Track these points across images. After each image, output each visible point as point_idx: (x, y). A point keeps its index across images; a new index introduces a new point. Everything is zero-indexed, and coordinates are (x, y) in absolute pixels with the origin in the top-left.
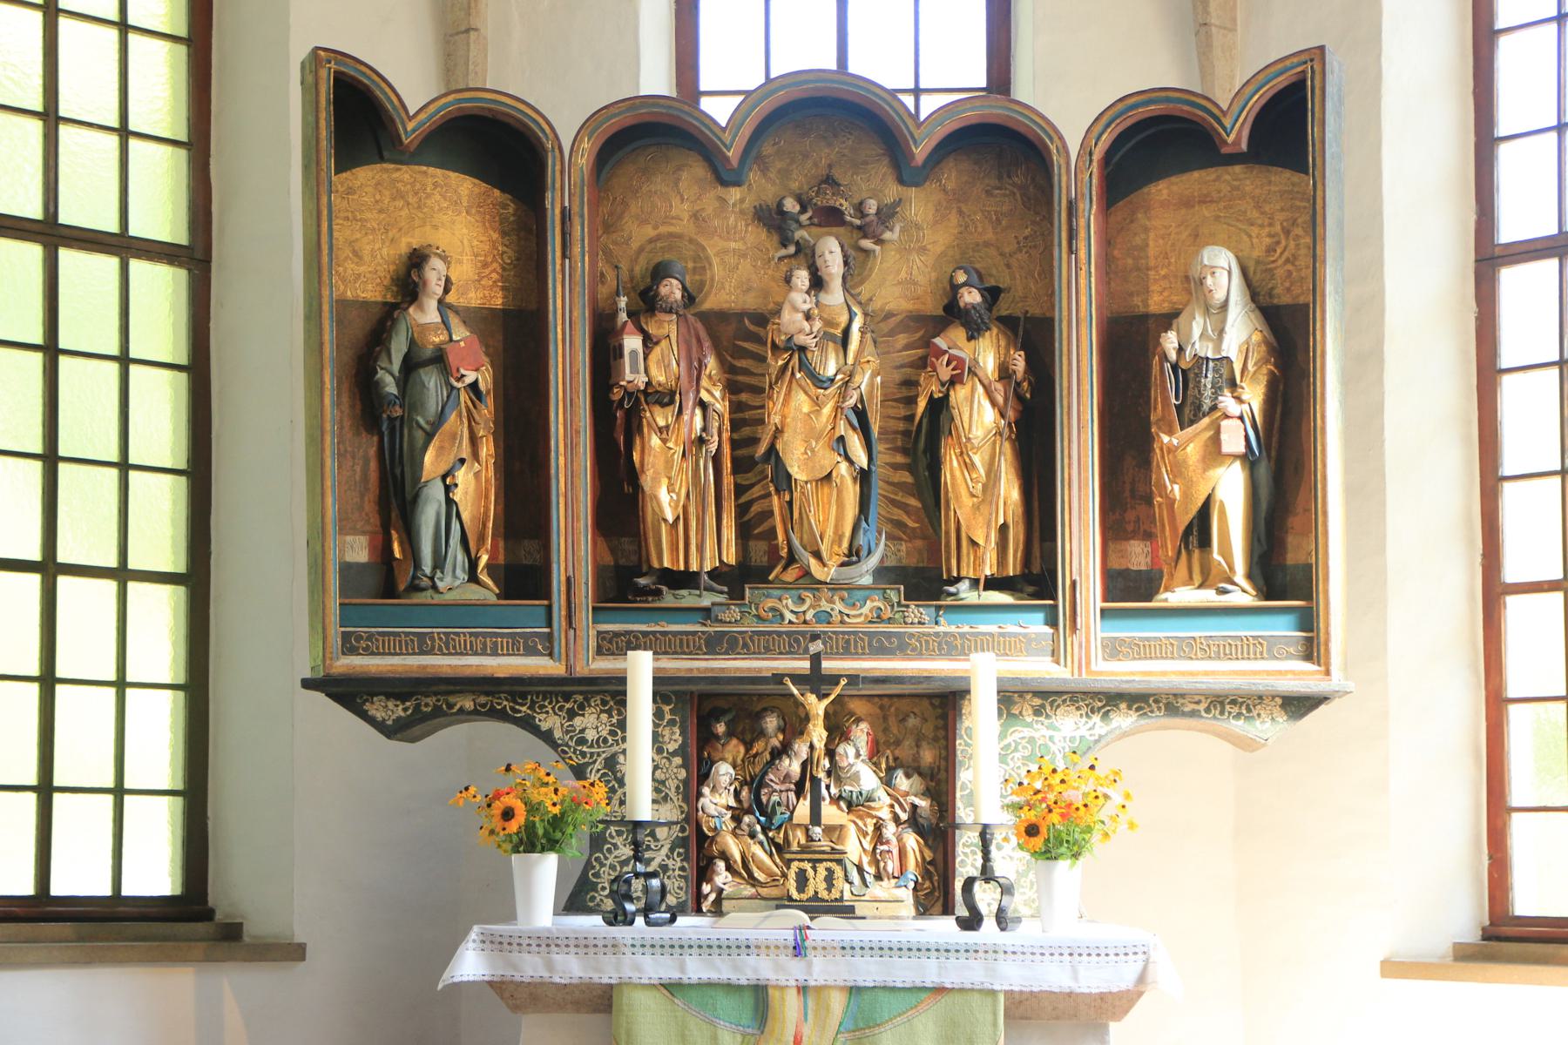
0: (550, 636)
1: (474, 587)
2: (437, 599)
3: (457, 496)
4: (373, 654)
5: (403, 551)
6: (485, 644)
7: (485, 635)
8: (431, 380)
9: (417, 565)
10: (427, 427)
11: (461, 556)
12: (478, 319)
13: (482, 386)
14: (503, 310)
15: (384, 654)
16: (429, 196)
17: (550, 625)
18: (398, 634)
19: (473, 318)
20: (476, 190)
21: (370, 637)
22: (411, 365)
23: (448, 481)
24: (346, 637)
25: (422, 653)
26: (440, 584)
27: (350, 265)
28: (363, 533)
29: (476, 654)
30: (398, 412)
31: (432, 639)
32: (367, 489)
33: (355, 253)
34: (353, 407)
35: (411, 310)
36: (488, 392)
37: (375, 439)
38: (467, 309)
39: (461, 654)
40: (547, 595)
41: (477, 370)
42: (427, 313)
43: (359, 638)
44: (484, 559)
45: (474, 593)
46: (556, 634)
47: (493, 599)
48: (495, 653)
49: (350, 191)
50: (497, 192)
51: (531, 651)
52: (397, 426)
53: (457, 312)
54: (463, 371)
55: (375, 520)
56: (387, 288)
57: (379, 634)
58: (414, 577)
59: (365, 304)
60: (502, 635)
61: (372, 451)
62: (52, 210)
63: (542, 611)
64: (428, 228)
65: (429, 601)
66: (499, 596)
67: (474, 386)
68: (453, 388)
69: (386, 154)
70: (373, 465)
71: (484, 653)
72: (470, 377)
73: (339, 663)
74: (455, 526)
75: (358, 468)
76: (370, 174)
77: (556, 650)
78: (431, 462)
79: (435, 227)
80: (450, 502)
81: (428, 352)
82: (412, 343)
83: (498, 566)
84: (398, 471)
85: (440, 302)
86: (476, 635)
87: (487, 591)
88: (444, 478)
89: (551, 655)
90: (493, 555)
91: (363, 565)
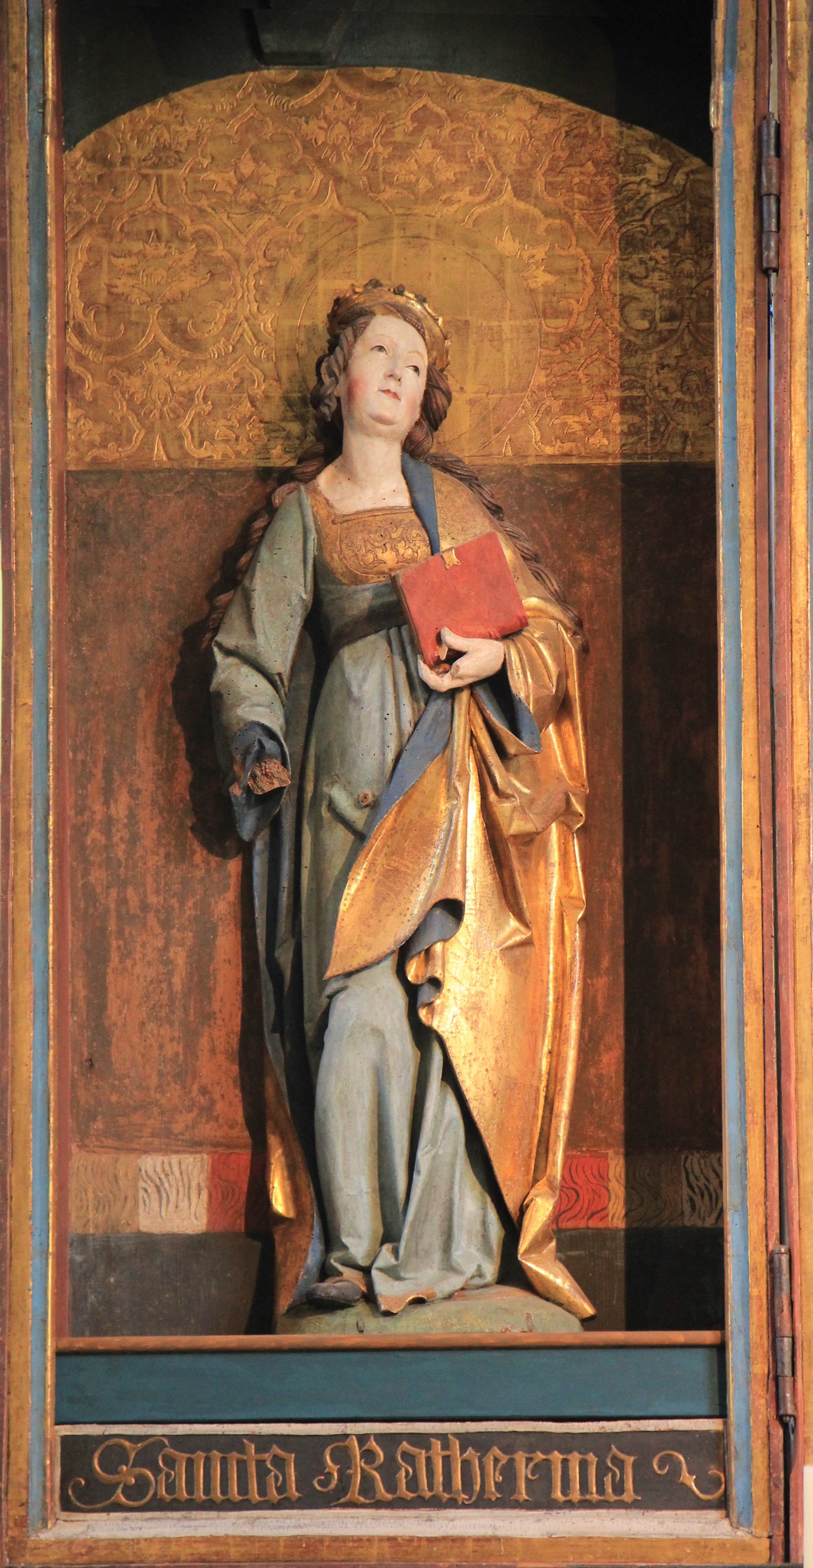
0: (716, 1448)
1: (513, 1295)
2: (377, 1331)
3: (447, 1018)
4: (158, 1505)
5: (295, 1195)
6: (509, 1471)
7: (509, 1443)
8: (368, 673)
9: (330, 1239)
10: (357, 817)
11: (471, 1203)
12: (538, 503)
13: (521, 686)
14: (625, 469)
15: (191, 1505)
16: (401, 151)
17: (722, 1413)
18: (235, 1443)
19: (506, 495)
20: (546, 124)
21: (149, 1453)
22: (323, 637)
23: (413, 972)
24: (74, 1452)
25: (311, 1500)
26: (383, 1286)
27: (161, 368)
28: (194, 1146)
29: (481, 1503)
30: (275, 776)
31: (343, 1457)
32: (207, 1017)
33: (177, 332)
34: (167, 776)
35: (323, 480)
36: (561, 707)
37: (234, 866)
38: (512, 474)
39: (435, 1503)
40: (713, 1317)
41: (509, 635)
42: (372, 480)
43: (114, 1454)
44: (541, 1211)
45: (507, 1315)
46: (736, 1438)
47: (567, 1329)
48: (541, 1501)
49: (165, 155)
50: (609, 124)
51: (659, 1493)
52: (289, 815)
53: (470, 479)
54: (453, 639)
55: (231, 1106)
56: (271, 428)
57: (178, 1441)
58: (325, 1272)
59: (207, 476)
60: (566, 1443)
61: (224, 905)
62: (506, 874)
63: (699, 1365)
64: (396, 246)
65: (352, 1338)
66: (587, 1323)
67: (497, 684)
68: (430, 692)
69: (270, 41)
70: (227, 943)
71: (506, 1500)
72: (481, 656)
73: (46, 1536)
74: (440, 1107)
75: (180, 956)
76: (224, 103)
77: (737, 1490)
78: (362, 918)
79: (417, 240)
80: (424, 1037)
81: (362, 600)
82: (321, 574)
83: (602, 1236)
84: (285, 957)
85: (411, 449)
86: (480, 1443)
87: (559, 1304)
88: (404, 953)
89: (723, 1504)
90: (569, 1194)
91: (190, 1246)
